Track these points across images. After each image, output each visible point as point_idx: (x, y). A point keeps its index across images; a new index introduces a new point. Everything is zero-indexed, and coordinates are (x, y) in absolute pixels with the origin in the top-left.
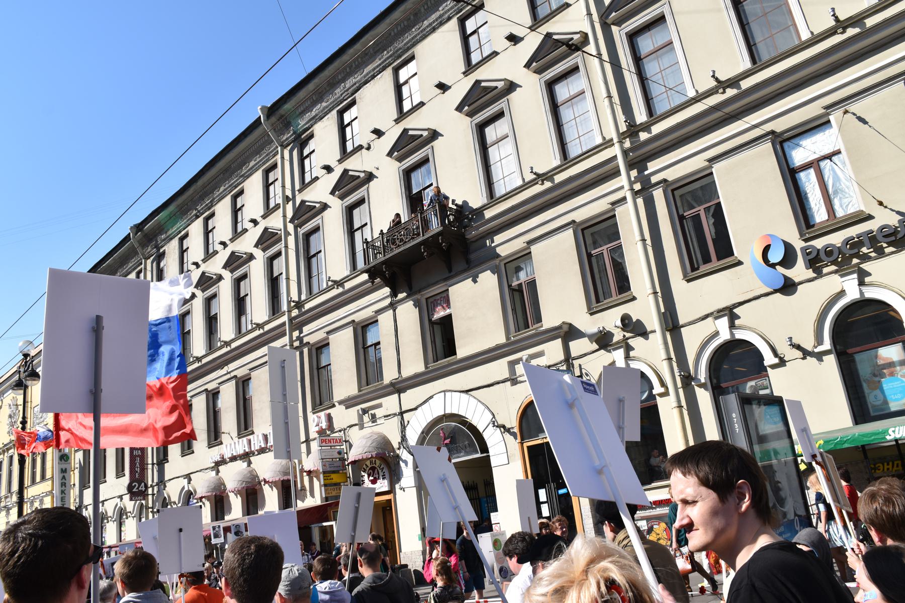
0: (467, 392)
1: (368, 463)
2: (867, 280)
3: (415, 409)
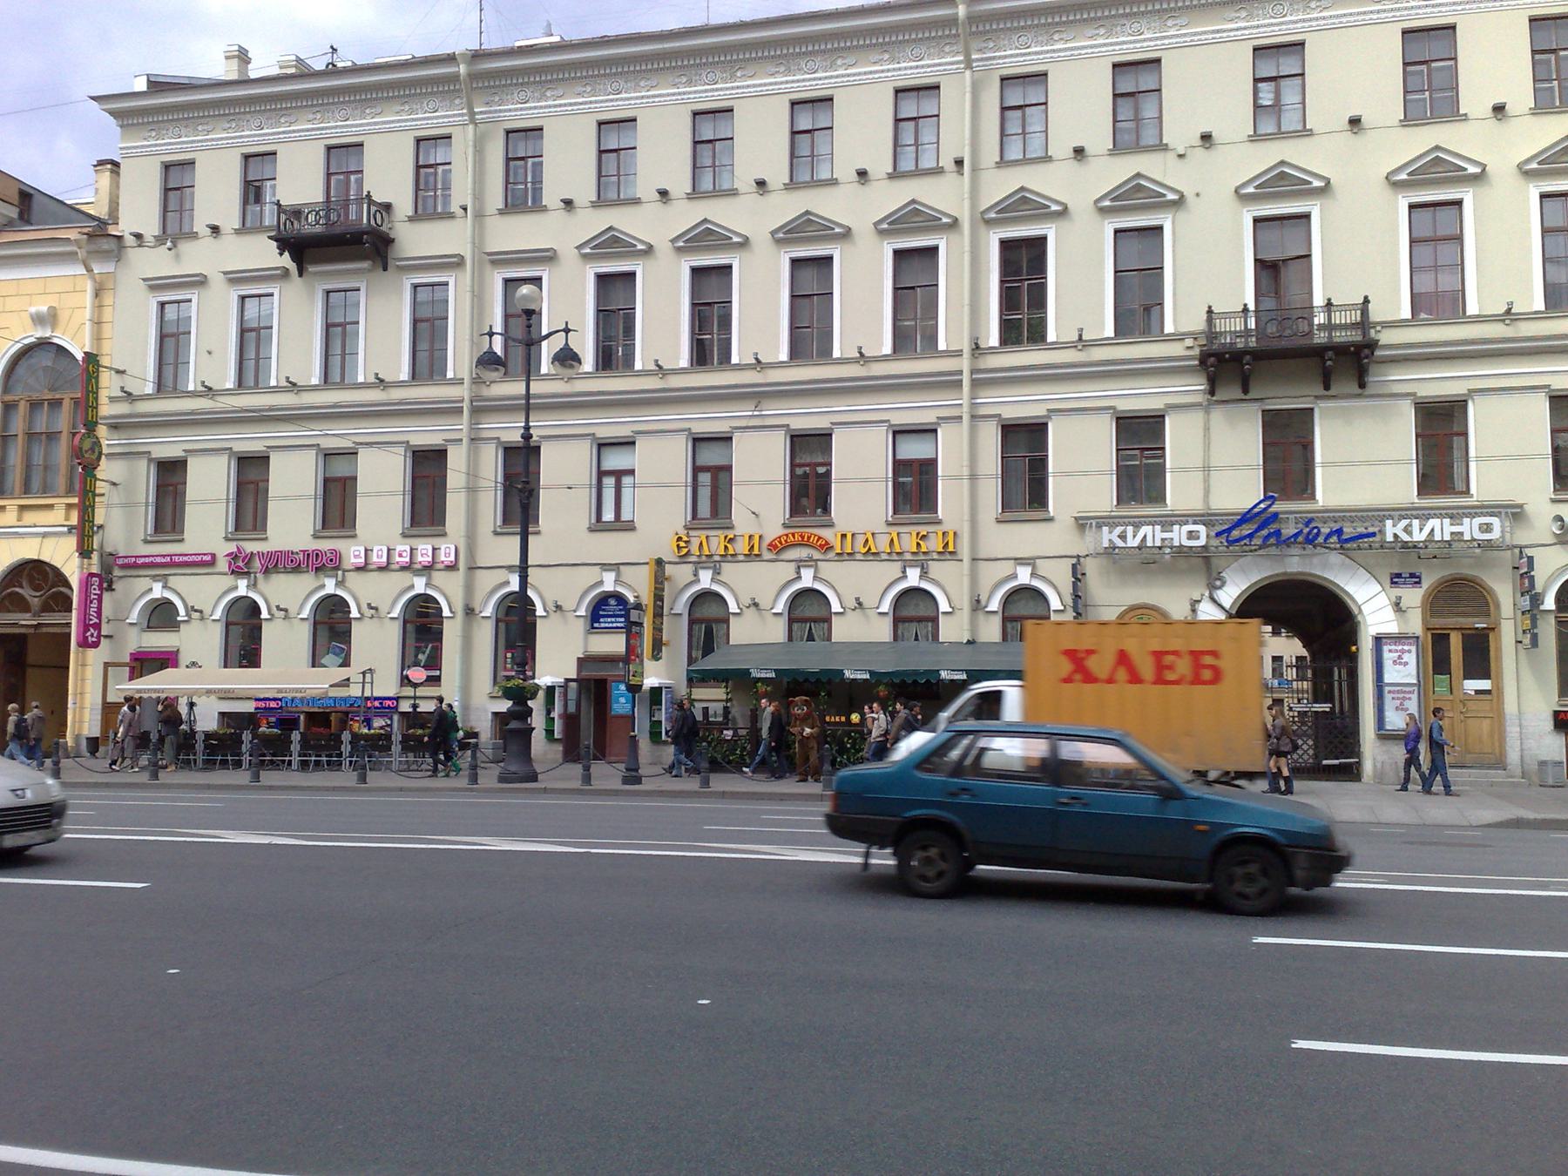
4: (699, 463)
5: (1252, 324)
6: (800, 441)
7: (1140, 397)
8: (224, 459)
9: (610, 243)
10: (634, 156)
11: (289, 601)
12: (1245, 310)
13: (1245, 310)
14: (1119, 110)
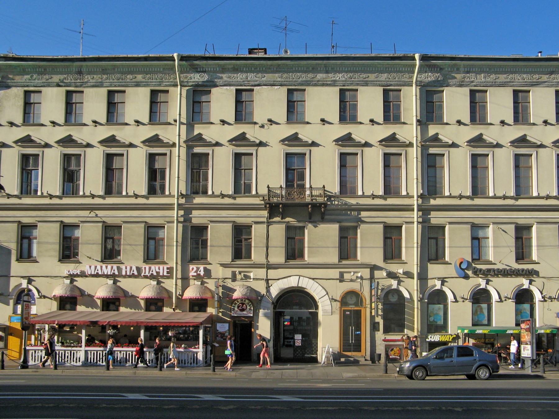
0: (313, 279)
1: (239, 301)
2: (490, 283)
3: (278, 279)
4: (149, 236)
5: (284, 193)
6: (65, 227)
7: (243, 217)
8: (101, 224)
9: (27, 141)
10: (40, 106)
11: (501, 288)
12: (281, 187)
13: (281, 187)
14: (238, 107)
